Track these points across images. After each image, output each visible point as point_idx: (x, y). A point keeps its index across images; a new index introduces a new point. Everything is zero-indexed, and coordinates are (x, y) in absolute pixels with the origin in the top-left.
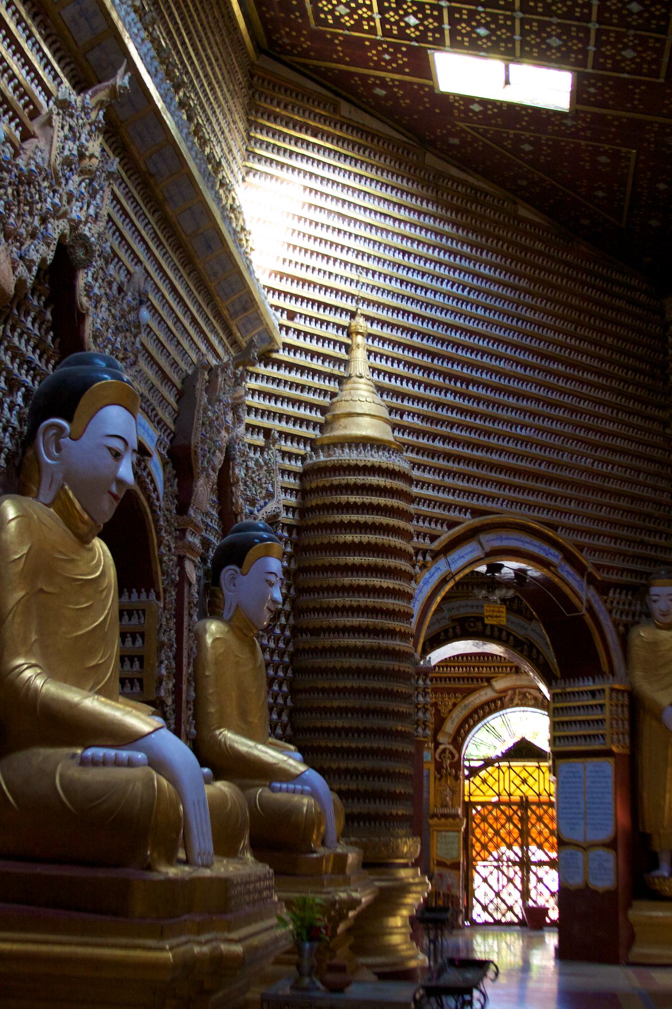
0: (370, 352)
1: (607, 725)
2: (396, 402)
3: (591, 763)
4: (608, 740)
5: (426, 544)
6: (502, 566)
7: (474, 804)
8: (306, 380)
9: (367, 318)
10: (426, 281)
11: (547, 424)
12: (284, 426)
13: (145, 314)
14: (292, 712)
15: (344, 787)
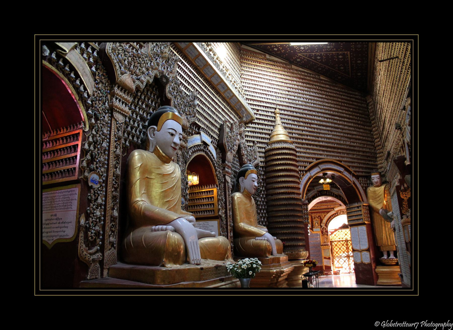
0: (281, 118)
1: (363, 216)
2: (290, 131)
3: (360, 227)
4: (364, 219)
5: (303, 169)
6: (327, 174)
7: (333, 242)
8: (263, 127)
9: (279, 109)
10: (296, 98)
11: (335, 133)
12: (258, 140)
13: (197, 102)
14: (268, 218)
15: (283, 238)
